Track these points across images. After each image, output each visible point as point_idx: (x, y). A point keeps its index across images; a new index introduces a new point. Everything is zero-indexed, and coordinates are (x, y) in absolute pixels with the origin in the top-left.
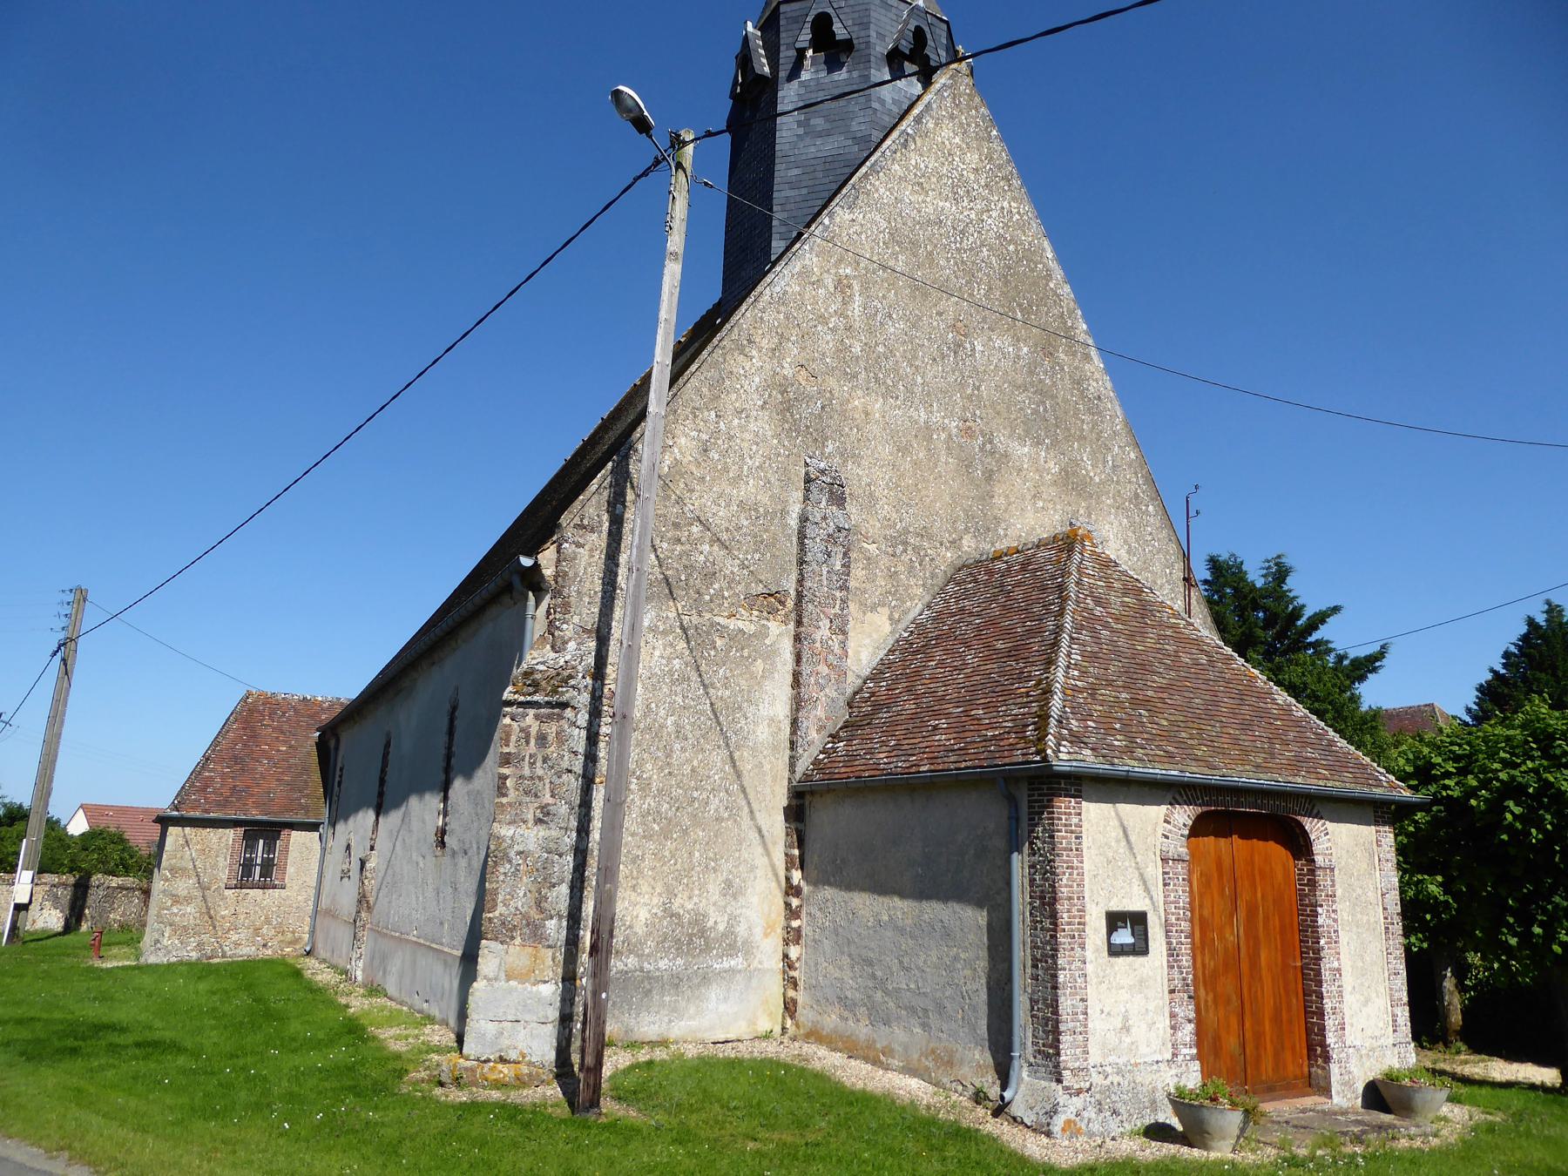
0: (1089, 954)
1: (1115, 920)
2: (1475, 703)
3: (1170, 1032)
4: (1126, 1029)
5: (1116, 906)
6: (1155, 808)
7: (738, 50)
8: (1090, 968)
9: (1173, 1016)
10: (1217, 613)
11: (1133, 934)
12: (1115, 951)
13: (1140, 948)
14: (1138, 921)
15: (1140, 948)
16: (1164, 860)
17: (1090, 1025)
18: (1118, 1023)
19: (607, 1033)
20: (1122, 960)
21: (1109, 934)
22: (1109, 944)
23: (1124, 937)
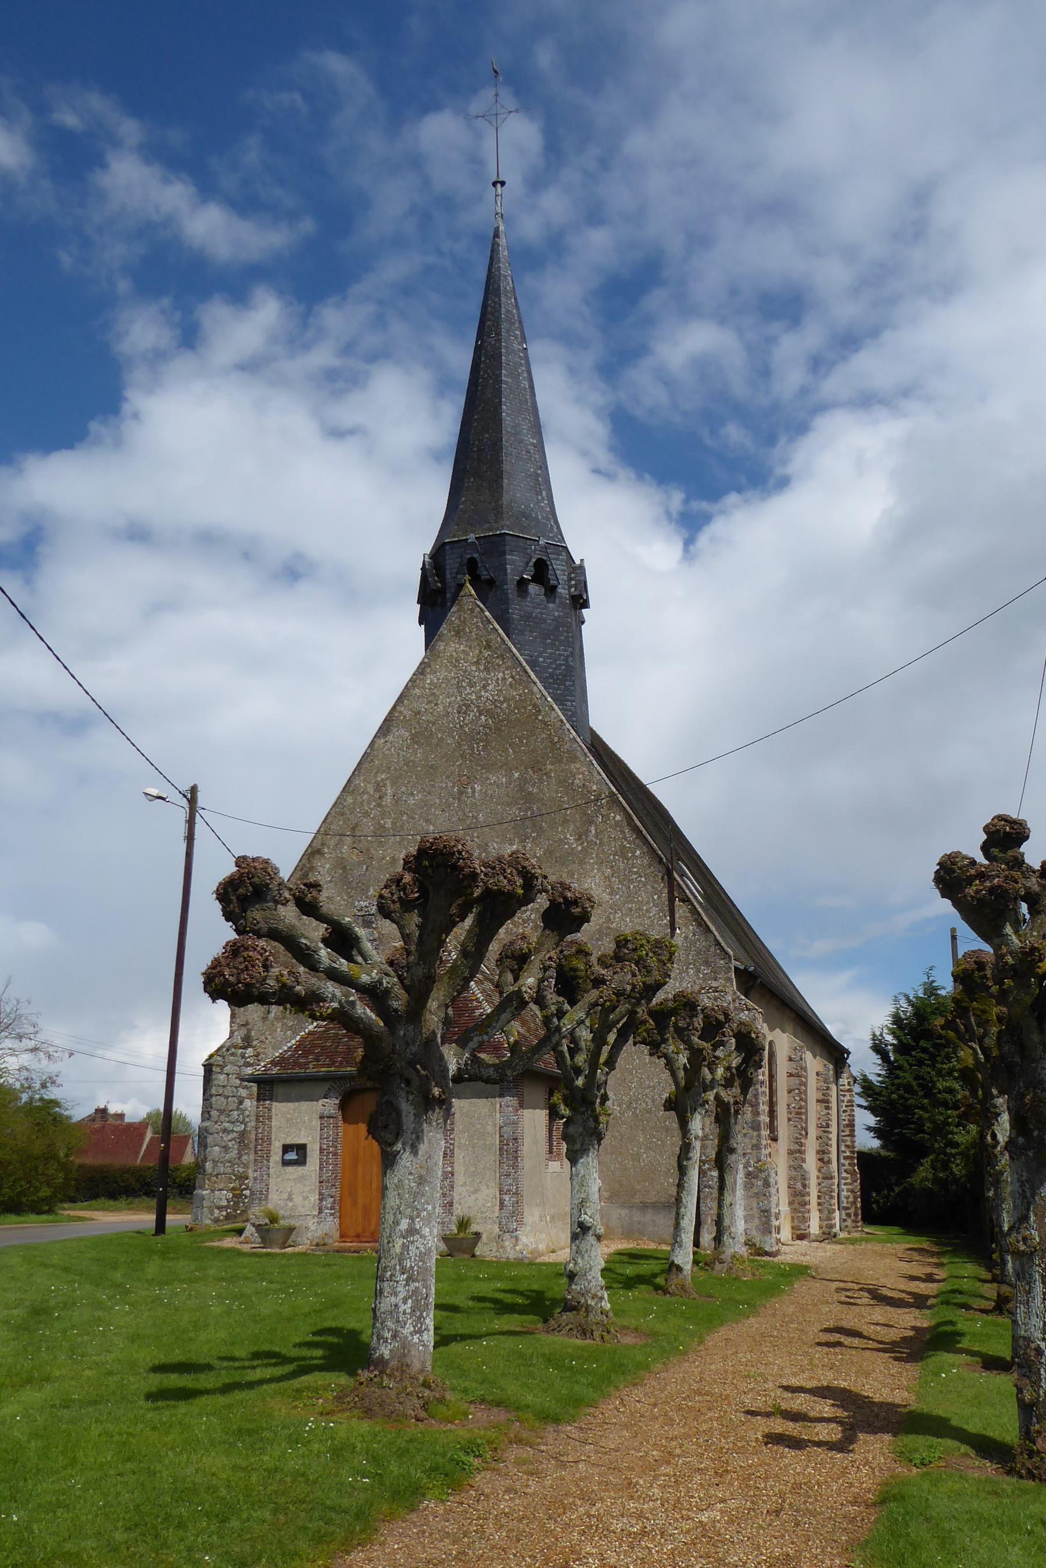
0: (271, 1164)
1: (286, 1149)
2: (878, 1048)
3: (318, 1201)
4: (290, 1199)
5: (289, 1141)
6: (651, 790)
7: (421, 566)
8: (271, 1171)
9: (320, 1194)
10: (381, 903)
11: (297, 1154)
12: (286, 1163)
13: (301, 1161)
14: (301, 1149)
15: (301, 1161)
16: (321, 1118)
17: (270, 1197)
18: (285, 1196)
19: (174, 1109)
20: (290, 1169)
21: (284, 1154)
22: (283, 1159)
23: (292, 1156)
